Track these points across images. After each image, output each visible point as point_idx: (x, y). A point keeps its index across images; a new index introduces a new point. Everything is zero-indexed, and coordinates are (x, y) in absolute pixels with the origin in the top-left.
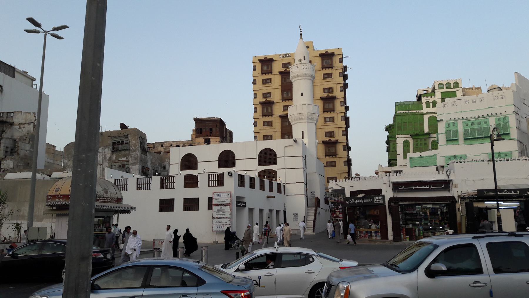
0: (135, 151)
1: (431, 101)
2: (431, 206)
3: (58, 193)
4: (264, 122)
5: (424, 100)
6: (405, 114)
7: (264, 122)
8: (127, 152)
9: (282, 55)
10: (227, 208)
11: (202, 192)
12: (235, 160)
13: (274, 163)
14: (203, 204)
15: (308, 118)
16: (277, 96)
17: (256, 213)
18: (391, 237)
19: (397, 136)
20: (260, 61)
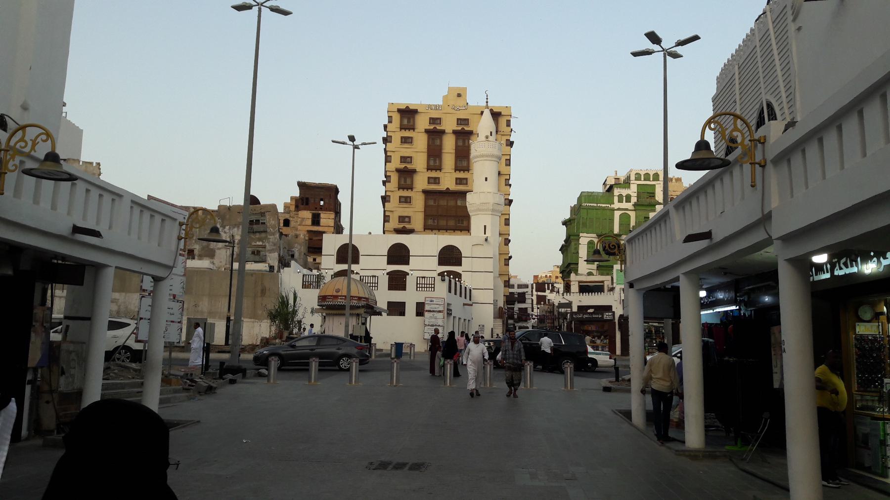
0: (273, 234)
1: (624, 195)
2: (656, 324)
3: (339, 294)
4: (400, 197)
5: (617, 192)
6: (593, 208)
7: (400, 197)
8: (263, 235)
9: (430, 106)
10: (440, 315)
11: (410, 297)
12: (409, 256)
13: (459, 264)
14: (411, 309)
15: (493, 210)
16: (420, 162)
17: (457, 319)
18: (618, 352)
19: (581, 235)
20: (400, 111)
